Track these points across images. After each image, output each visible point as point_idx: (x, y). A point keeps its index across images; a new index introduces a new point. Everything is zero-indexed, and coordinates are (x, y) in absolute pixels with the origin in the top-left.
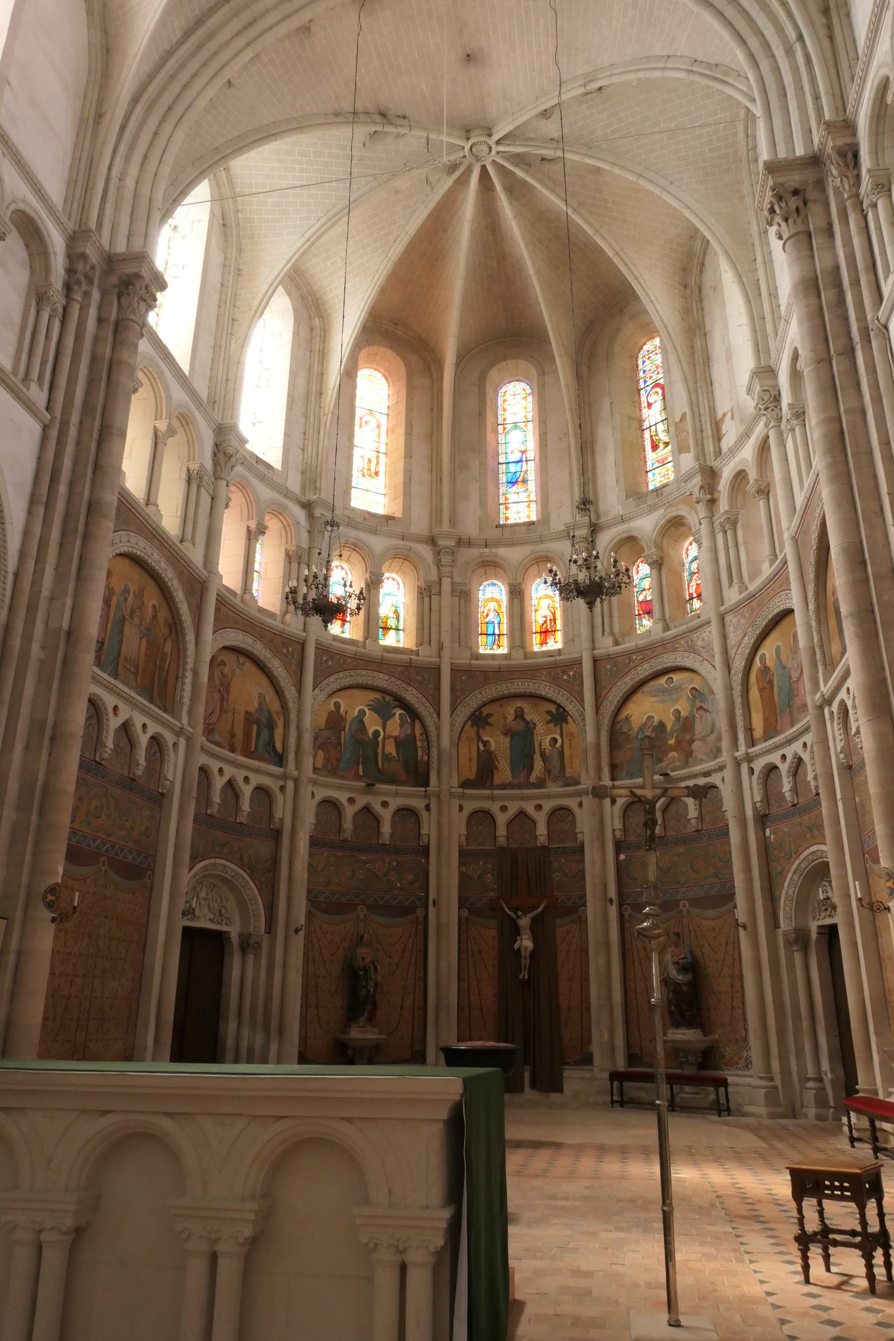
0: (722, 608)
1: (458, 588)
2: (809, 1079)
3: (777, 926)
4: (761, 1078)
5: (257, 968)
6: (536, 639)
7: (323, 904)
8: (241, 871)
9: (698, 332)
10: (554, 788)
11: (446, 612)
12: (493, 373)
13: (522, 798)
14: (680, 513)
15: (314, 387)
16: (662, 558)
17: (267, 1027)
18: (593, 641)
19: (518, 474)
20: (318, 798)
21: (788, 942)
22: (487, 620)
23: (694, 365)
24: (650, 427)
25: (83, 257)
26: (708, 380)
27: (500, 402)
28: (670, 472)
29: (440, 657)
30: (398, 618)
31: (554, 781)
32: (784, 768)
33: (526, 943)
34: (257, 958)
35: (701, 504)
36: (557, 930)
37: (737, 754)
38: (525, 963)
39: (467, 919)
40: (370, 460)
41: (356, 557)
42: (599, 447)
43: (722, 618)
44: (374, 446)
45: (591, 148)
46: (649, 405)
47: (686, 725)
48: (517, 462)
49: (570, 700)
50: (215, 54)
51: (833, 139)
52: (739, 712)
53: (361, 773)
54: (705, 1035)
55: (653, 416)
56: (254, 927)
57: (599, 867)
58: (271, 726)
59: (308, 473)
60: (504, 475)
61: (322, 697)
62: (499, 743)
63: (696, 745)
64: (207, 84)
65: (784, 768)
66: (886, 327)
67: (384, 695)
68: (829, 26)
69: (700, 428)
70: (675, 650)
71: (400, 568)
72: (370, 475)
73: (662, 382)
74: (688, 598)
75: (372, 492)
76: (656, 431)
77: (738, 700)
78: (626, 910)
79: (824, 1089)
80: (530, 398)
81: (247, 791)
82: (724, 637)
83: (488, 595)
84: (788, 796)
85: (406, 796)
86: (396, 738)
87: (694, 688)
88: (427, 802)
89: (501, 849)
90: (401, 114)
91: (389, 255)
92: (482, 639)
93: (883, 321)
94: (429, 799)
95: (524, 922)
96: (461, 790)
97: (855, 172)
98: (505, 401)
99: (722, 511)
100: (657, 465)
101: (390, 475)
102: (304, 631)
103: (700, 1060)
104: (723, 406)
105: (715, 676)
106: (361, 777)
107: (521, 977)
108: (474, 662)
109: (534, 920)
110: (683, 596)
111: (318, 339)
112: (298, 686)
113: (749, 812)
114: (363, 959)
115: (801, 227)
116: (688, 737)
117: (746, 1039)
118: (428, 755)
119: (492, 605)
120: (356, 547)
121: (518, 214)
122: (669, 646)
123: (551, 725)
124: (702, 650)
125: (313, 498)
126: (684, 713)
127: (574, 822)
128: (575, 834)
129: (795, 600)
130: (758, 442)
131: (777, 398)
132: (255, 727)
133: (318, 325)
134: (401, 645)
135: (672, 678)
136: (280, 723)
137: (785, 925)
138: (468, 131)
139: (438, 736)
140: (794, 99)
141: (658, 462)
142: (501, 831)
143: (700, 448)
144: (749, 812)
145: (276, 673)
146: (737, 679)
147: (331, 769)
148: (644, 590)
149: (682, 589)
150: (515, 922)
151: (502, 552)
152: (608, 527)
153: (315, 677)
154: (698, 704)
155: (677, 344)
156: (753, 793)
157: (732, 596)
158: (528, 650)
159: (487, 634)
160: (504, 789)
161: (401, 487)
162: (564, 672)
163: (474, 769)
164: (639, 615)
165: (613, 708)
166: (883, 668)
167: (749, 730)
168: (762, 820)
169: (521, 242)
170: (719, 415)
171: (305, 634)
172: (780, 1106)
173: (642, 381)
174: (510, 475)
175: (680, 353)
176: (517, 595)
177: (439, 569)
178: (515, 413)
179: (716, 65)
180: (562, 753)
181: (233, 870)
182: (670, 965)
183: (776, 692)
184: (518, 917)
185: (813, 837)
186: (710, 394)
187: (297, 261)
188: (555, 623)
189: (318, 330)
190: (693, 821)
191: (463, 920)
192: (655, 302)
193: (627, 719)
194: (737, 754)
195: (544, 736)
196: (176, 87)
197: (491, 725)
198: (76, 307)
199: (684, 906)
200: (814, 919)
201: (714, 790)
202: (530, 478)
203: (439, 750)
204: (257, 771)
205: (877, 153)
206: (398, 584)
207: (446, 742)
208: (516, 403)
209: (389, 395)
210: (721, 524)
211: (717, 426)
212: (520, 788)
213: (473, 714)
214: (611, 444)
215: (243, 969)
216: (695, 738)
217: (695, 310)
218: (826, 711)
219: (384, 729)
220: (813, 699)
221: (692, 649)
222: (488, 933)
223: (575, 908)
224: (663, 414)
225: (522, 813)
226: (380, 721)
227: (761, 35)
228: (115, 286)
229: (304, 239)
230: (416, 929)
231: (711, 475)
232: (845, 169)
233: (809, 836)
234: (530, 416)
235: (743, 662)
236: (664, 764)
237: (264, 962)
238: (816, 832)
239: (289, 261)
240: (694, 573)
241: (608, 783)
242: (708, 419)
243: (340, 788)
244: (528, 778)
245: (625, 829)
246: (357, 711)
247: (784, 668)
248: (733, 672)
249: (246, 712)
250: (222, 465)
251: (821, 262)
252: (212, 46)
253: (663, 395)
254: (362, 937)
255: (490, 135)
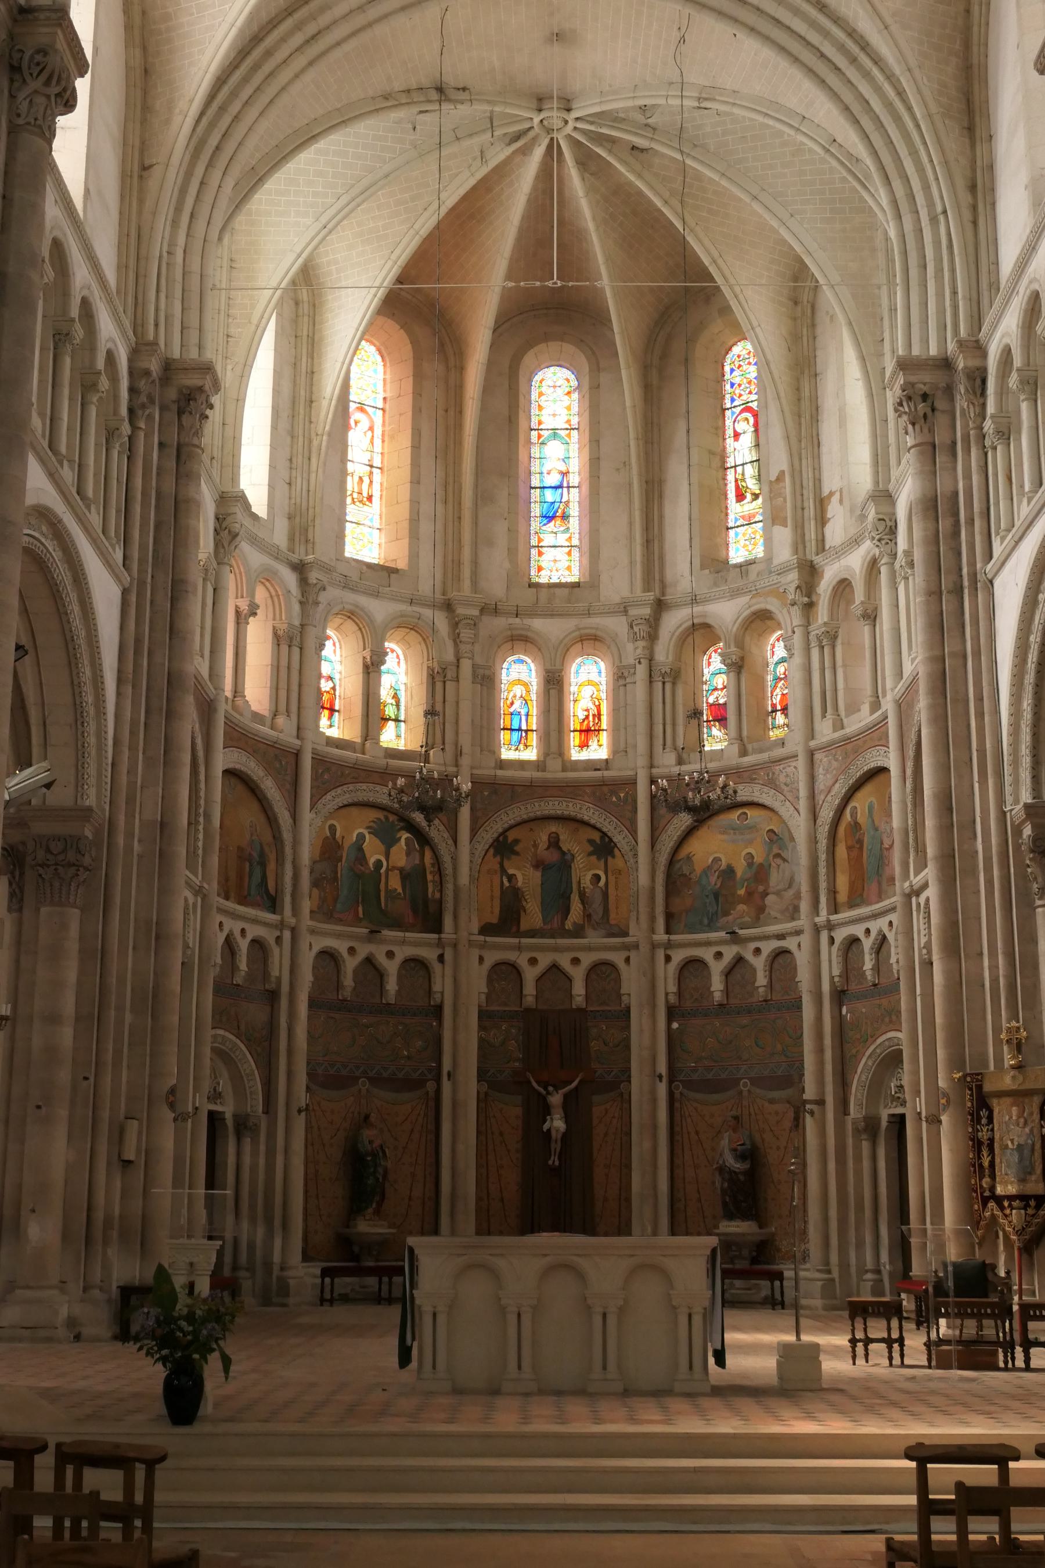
0: (812, 744)
1: (481, 672)
2: (867, 1271)
3: (846, 1112)
4: (818, 1270)
5: (255, 1154)
6: (575, 739)
7: (326, 1078)
8: (238, 1042)
9: (806, 372)
10: (594, 938)
11: (465, 707)
12: (529, 359)
13: (556, 949)
14: (769, 607)
15: (302, 393)
16: (742, 659)
17: (269, 1220)
18: (651, 756)
19: (557, 505)
20: (316, 949)
21: (857, 1131)
22: (512, 710)
23: (800, 416)
24: (735, 466)
25: (147, 373)
26: (815, 439)
27: (534, 396)
28: (758, 537)
29: (457, 766)
30: (398, 705)
31: (595, 929)
32: (867, 944)
33: (557, 1124)
34: (255, 1142)
35: (796, 607)
36: (594, 1109)
37: (817, 920)
38: (555, 1147)
39: (486, 1094)
40: (361, 478)
41: (350, 626)
42: (668, 489)
43: (811, 754)
44: (365, 458)
45: (695, 146)
46: (737, 435)
47: (760, 873)
48: (556, 488)
49: (619, 829)
50: (271, 75)
51: (965, 358)
52: (822, 871)
53: (361, 915)
54: (760, 1227)
55: (741, 450)
56: (252, 1106)
57: (647, 1037)
58: (263, 864)
59: (298, 519)
60: (537, 505)
61: (318, 822)
62: (527, 877)
63: (770, 899)
64: (261, 114)
65: (867, 944)
66: (991, 582)
67: (386, 813)
68: (974, 208)
69: (799, 500)
70: (752, 780)
71: (403, 638)
72: (361, 502)
73: (754, 405)
74: (770, 709)
75: (368, 536)
76: (743, 474)
77: (823, 857)
78: (677, 1087)
79: (882, 1281)
80: (575, 396)
81: (243, 945)
82: (812, 778)
83: (514, 676)
84: (869, 974)
85: (417, 944)
86: (401, 870)
87: (771, 831)
88: (440, 952)
89: (528, 1010)
90: (461, 86)
91: (417, 226)
92: (504, 736)
93: (990, 576)
94: (444, 948)
95: (556, 1099)
96: (482, 938)
97: (981, 401)
98: (541, 394)
99: (820, 621)
100: (740, 522)
101: (390, 502)
102: (298, 737)
103: (754, 1254)
104: (830, 483)
105: (798, 824)
106: (361, 919)
107: (550, 1162)
108: (500, 773)
109: (566, 1097)
110: (765, 706)
111: (306, 319)
112: (292, 810)
113: (826, 987)
114: (371, 1142)
115: (927, 438)
116: (761, 888)
117: (804, 1232)
118: (441, 891)
119: (519, 690)
120: (352, 615)
121: (590, 190)
122: (746, 775)
123: (594, 858)
124: (786, 788)
125: (310, 558)
126: (758, 859)
127: (618, 980)
128: (619, 996)
129: (892, 763)
130: (866, 564)
131: (893, 531)
132: (247, 865)
133: (305, 298)
134: (402, 747)
135: (745, 813)
136: (272, 857)
137: (855, 1112)
138: (540, 100)
139: (455, 868)
140: (933, 280)
141: (743, 517)
142: (530, 989)
143: (799, 531)
144: (826, 987)
145: (269, 796)
146: (823, 832)
147: (325, 912)
148: (716, 689)
149: (764, 698)
150: (545, 1099)
151: (538, 624)
152: (678, 606)
153: (312, 796)
154: (775, 851)
155: (781, 389)
156: (831, 966)
157: (825, 731)
158: (566, 758)
159: (511, 730)
160: (533, 937)
161: (406, 525)
162: (614, 793)
163: (497, 910)
164: (708, 721)
165: (672, 843)
166: (957, 912)
167: (833, 892)
168: (840, 996)
169: (600, 259)
170: (826, 492)
171: (298, 742)
172: (836, 1298)
173: (728, 397)
174: (546, 505)
175: (784, 401)
176: (554, 684)
177: (456, 645)
178: (554, 415)
179: (857, 160)
180: (605, 895)
181: (231, 1041)
182: (727, 1151)
183: (865, 855)
184: (548, 1093)
185: (891, 1021)
186: (816, 460)
187: (311, 254)
188: (599, 719)
189: (306, 305)
190: (761, 990)
191: (482, 1096)
192: (758, 330)
193: (689, 858)
194: (817, 920)
195: (585, 871)
196: (226, 120)
197: (517, 854)
198: (142, 434)
199: (745, 1086)
200: (885, 1107)
201: (788, 955)
202: (572, 513)
203: (455, 885)
204: (255, 921)
205: (1002, 394)
206: (398, 657)
207: (464, 879)
208: (555, 395)
209: (385, 380)
210: (818, 637)
211: (822, 504)
212: (553, 937)
213: (497, 840)
214: (684, 489)
215: (239, 1154)
216: (771, 890)
217: (805, 339)
218: (914, 899)
219: (387, 860)
220: (902, 886)
221: (772, 783)
222: (511, 1111)
223: (617, 1084)
224: (753, 452)
225: (555, 967)
226: (382, 848)
227: (907, 180)
228: (174, 402)
229: (319, 225)
230: (621, 1109)
231: (810, 572)
232: (972, 397)
233: (887, 1019)
234: (575, 421)
235: (832, 814)
236: (730, 918)
237: (262, 1148)
238: (894, 1018)
239: (299, 256)
240: (781, 679)
241: (661, 936)
242: (812, 496)
243: (339, 936)
244: (563, 924)
245: (680, 994)
246: (355, 836)
247: (876, 829)
248: (819, 822)
249: (239, 848)
250: (226, 545)
251: (942, 485)
252: (267, 68)
253: (756, 425)
254: (367, 1117)
255: (569, 110)
